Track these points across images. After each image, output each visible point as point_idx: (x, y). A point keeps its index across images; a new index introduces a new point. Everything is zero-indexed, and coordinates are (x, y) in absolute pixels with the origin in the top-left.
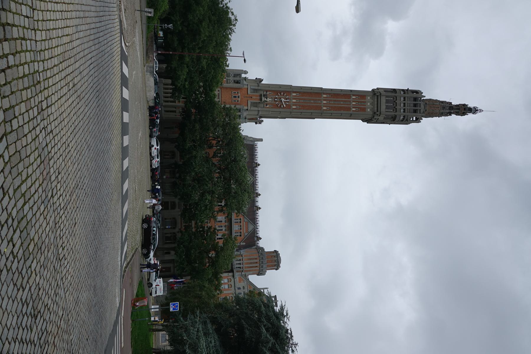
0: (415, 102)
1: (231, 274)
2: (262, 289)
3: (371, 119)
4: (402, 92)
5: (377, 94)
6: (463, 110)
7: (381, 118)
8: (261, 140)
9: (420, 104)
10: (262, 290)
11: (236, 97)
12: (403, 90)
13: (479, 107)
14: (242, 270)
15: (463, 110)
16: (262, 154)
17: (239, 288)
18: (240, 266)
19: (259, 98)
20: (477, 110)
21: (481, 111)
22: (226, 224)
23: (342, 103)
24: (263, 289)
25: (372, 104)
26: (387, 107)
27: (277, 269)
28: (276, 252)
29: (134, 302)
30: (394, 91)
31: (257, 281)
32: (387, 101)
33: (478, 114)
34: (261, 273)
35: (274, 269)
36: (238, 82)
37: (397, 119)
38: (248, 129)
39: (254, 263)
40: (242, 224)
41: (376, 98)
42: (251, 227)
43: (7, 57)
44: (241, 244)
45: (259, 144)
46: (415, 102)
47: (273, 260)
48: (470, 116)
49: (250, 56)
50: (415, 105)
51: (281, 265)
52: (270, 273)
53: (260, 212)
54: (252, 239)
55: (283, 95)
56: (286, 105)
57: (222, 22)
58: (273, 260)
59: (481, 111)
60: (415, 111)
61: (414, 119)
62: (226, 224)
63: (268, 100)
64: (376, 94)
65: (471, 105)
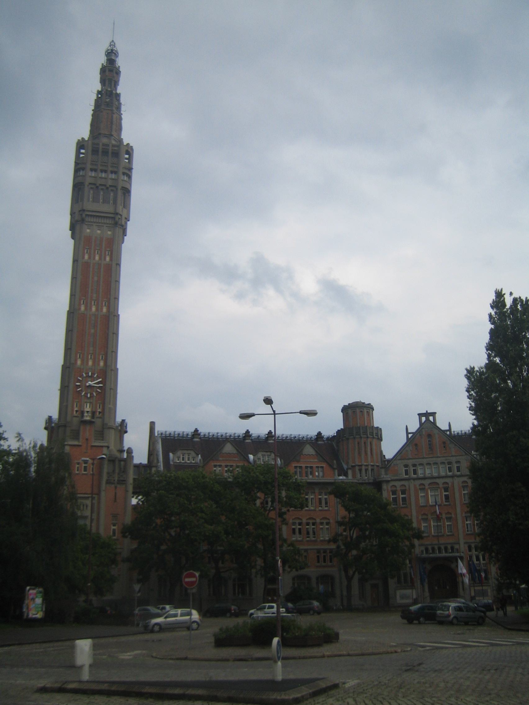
0: (100, 150)
1: (384, 486)
2: (407, 436)
3: (118, 223)
4: (81, 173)
5: (84, 216)
6: (110, 73)
9: (103, 145)
10: (410, 435)
11: (85, 467)
13: (105, 46)
14: (375, 467)
15: (110, 73)
16: (179, 422)
17: (407, 473)
18: (363, 471)
19: (88, 427)
20: (112, 50)
22: (317, 491)
23: (96, 279)
24: (408, 433)
26: (106, 201)
27: (373, 410)
28: (346, 410)
29: (285, 629)
31: (391, 447)
32: (95, 200)
33: (120, 48)
34: (377, 434)
35: (372, 414)
37: (127, 186)
39: (366, 448)
40: (315, 466)
41: (87, 219)
44: (335, 467)
45: (159, 428)
46: (100, 150)
47: (357, 414)
48: (120, 62)
51: (367, 403)
52: (378, 421)
53: (203, 430)
54: (328, 448)
55: (79, 381)
56: (98, 377)
60: (116, 154)
61: (127, 156)
62: (317, 491)
63: (88, 408)
65: (102, 60)
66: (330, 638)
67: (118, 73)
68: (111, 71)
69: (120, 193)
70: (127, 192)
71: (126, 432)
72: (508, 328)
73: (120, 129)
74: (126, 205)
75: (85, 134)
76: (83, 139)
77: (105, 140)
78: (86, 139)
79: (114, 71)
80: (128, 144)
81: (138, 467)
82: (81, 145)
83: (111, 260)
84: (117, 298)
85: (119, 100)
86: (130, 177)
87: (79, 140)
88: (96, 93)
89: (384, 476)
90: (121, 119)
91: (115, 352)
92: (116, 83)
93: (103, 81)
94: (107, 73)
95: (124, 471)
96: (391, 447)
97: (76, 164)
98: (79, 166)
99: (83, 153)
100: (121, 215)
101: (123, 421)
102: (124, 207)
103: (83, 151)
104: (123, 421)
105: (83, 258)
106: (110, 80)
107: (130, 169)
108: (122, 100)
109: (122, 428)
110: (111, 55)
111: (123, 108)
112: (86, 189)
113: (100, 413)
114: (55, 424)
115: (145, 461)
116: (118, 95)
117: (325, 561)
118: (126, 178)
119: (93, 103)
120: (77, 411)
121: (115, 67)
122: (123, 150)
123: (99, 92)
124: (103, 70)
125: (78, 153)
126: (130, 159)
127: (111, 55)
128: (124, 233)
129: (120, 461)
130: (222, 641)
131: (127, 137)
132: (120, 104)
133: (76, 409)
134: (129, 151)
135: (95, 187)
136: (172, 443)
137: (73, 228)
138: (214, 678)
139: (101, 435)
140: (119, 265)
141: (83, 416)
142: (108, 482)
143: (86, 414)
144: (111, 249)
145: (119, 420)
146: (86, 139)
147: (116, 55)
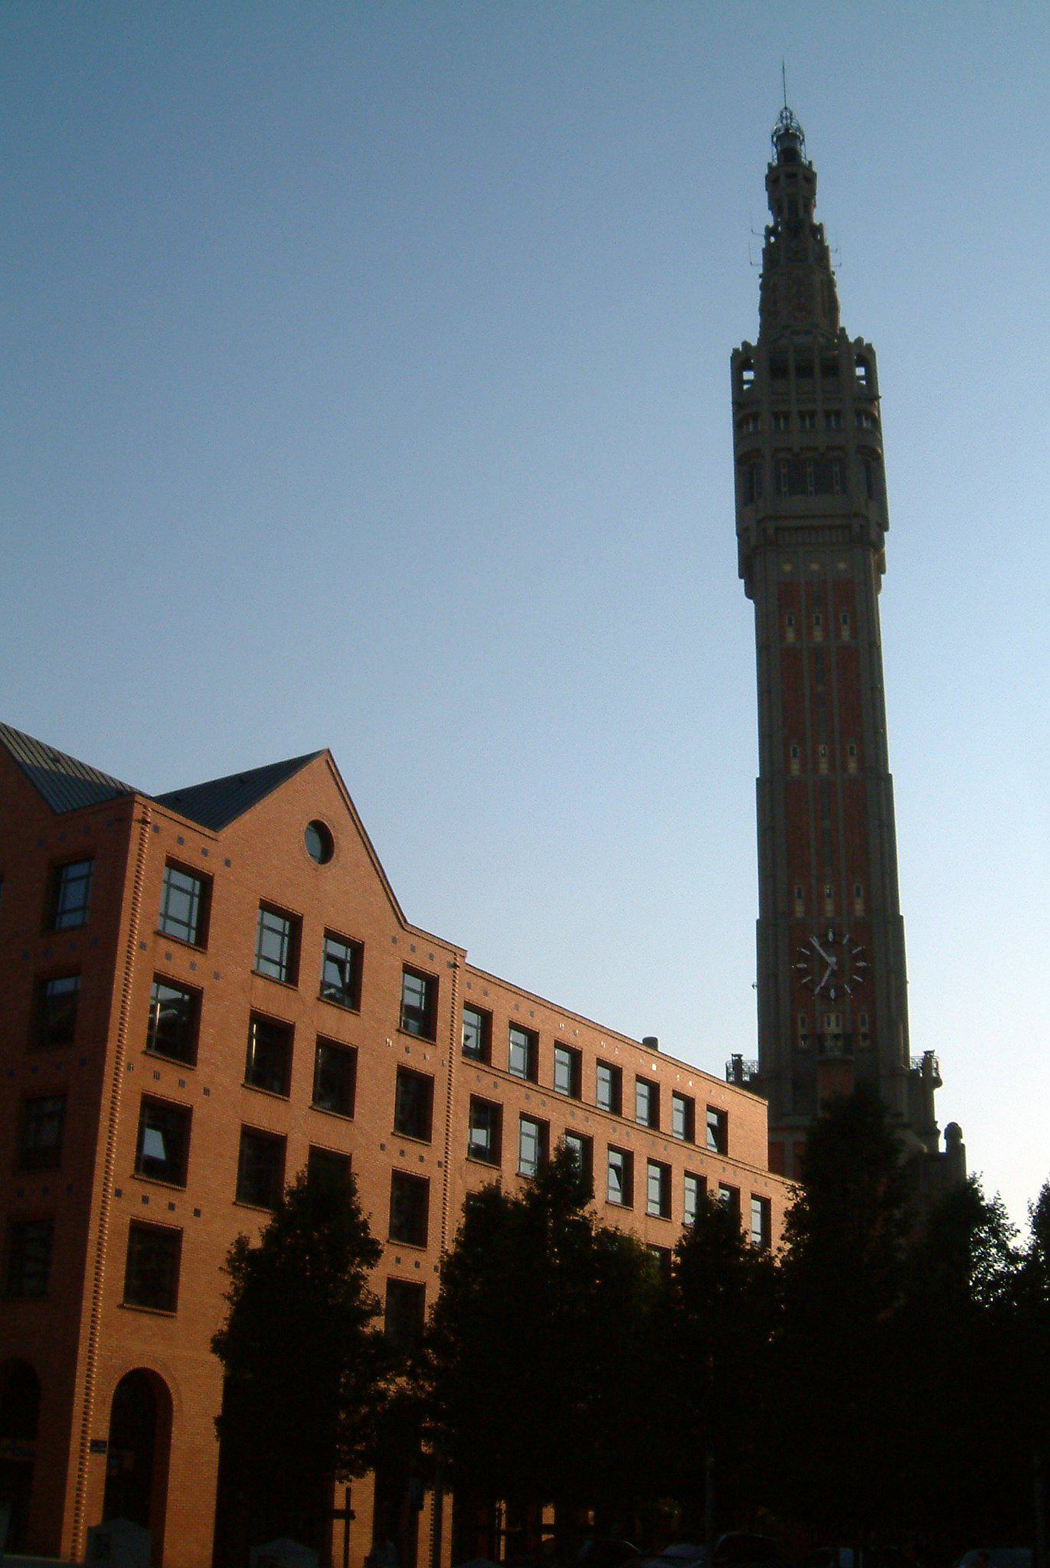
6: (791, 182)
13: (772, 124)
15: (791, 182)
33: (804, 121)
48: (809, 152)
61: (860, 371)
65: (769, 154)
68: (791, 176)
71: (938, 1082)
72: (575, 1160)
73: (831, 307)
76: (745, 344)
78: (754, 343)
79: (801, 176)
80: (859, 340)
82: (741, 360)
83: (854, 634)
87: (736, 351)
88: (763, 232)
93: (775, 205)
94: (783, 181)
98: (746, 411)
99: (747, 382)
100: (866, 518)
101: (929, 1056)
102: (870, 496)
103: (748, 375)
104: (929, 1056)
105: (783, 637)
108: (830, 240)
110: (788, 142)
111: (834, 260)
113: (865, 1037)
114: (752, 1075)
119: (759, 259)
120: (804, 1037)
121: (801, 164)
123: (770, 232)
124: (773, 180)
125: (737, 381)
127: (788, 142)
133: (801, 1031)
134: (865, 355)
137: (747, 569)
138: (596, 1183)
141: (822, 1049)
143: (829, 1043)
146: (754, 343)
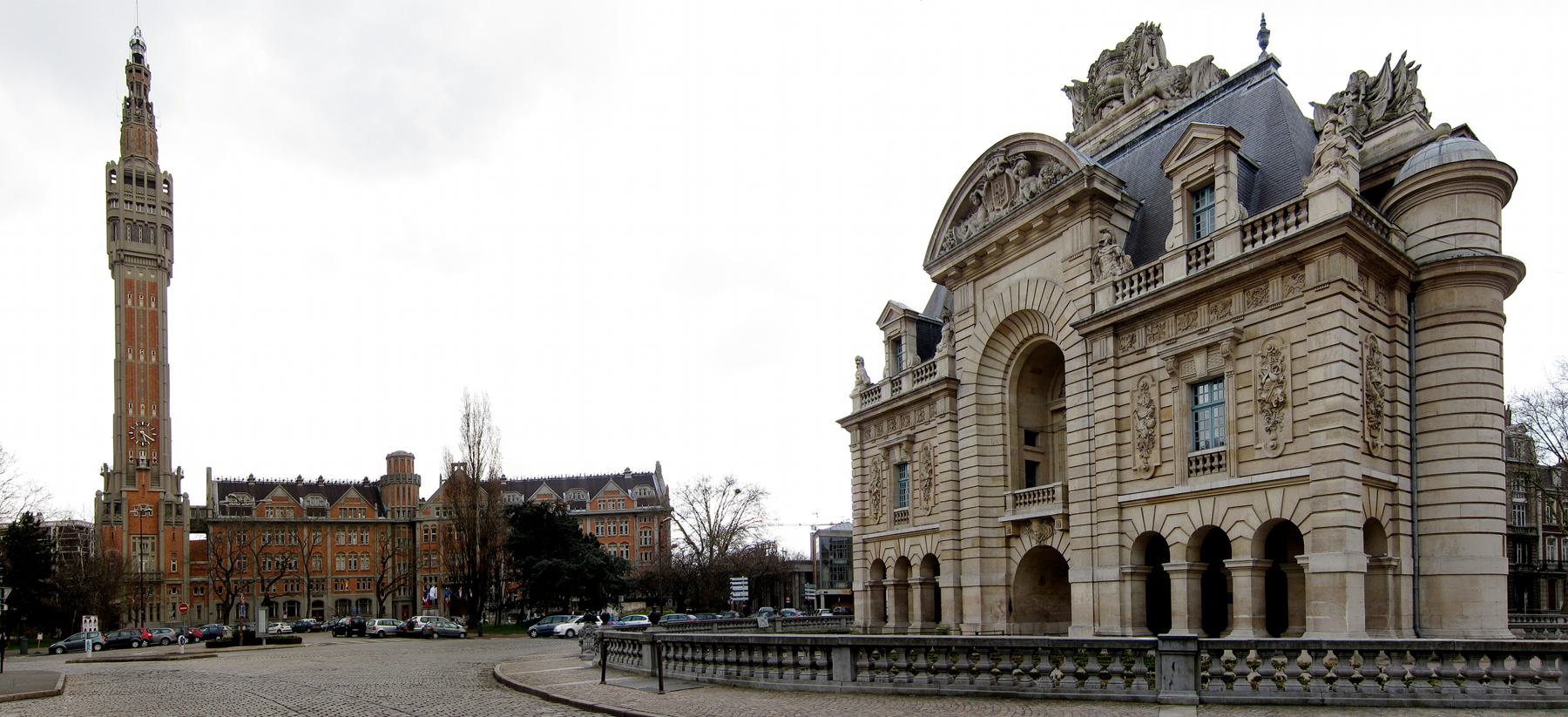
3: (163, 266)
4: (114, 205)
6: (137, 73)
7: (123, 209)
8: (209, 471)
12: (109, 202)
13: (129, 36)
15: (137, 73)
21: (137, 31)
25: (141, 267)
28: (389, 458)
30: (112, 221)
31: (429, 488)
32: (134, 238)
34: (417, 481)
36: (118, 508)
38: (196, 493)
41: (128, 260)
42: (353, 494)
43: (653, 675)
45: (220, 474)
47: (400, 464)
48: (149, 59)
49: (58, 475)
50: (140, 181)
53: (327, 479)
54: (370, 492)
57: (28, 532)
58: (400, 464)
59: (137, 31)
60: (152, 184)
63: (143, 457)
64: (118, 261)
65: (127, 54)
66: (299, 641)
67: (147, 75)
69: (160, 231)
70: (169, 230)
74: (169, 245)
75: (115, 155)
77: (893, 438)
81: (194, 509)
84: (165, 348)
85: (151, 112)
86: (171, 213)
89: (419, 516)
90: (155, 137)
91: (167, 402)
92: (147, 89)
93: (131, 85)
95: (179, 513)
96: (429, 488)
97: (109, 193)
106: (139, 85)
107: (171, 204)
109: (178, 477)
112: (122, 224)
115: (203, 503)
116: (149, 106)
117: (1212, 543)
118: (166, 214)
122: (159, 181)
126: (169, 188)
128: (170, 275)
129: (177, 506)
130: (1153, 547)
131: (165, 163)
132: (153, 117)
135: (134, 224)
136: (225, 488)
137: (112, 267)
139: (156, 479)
140: (165, 312)
142: (167, 523)
144: (156, 294)
145: (174, 468)
147: (144, 47)
